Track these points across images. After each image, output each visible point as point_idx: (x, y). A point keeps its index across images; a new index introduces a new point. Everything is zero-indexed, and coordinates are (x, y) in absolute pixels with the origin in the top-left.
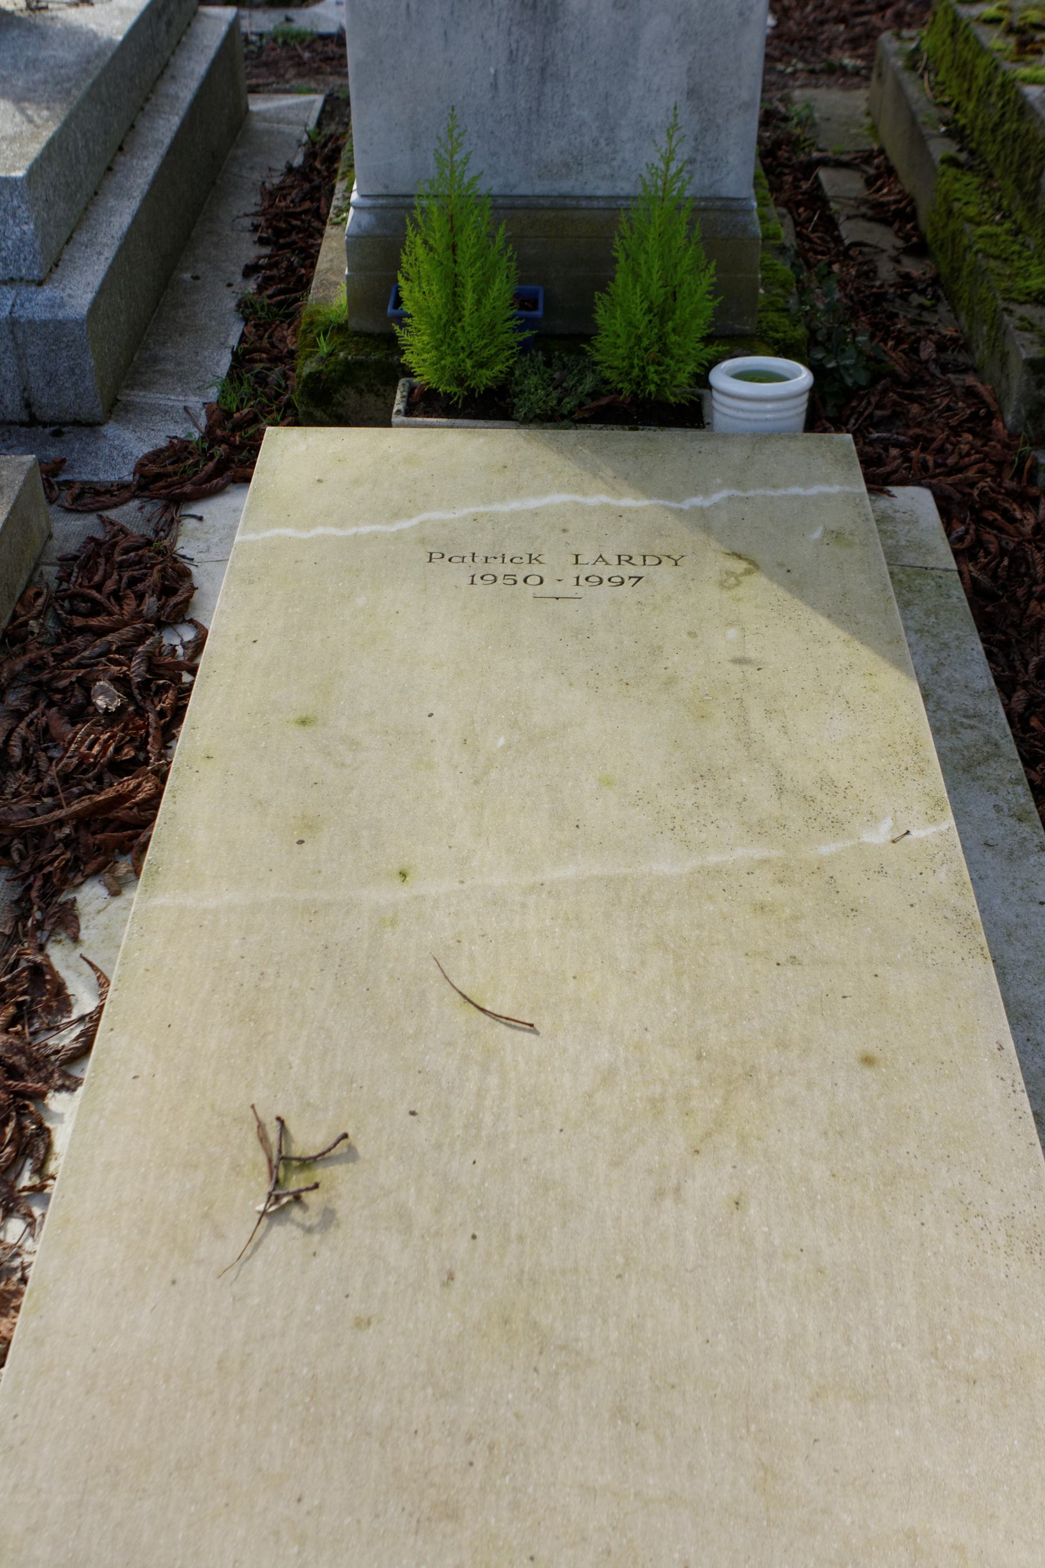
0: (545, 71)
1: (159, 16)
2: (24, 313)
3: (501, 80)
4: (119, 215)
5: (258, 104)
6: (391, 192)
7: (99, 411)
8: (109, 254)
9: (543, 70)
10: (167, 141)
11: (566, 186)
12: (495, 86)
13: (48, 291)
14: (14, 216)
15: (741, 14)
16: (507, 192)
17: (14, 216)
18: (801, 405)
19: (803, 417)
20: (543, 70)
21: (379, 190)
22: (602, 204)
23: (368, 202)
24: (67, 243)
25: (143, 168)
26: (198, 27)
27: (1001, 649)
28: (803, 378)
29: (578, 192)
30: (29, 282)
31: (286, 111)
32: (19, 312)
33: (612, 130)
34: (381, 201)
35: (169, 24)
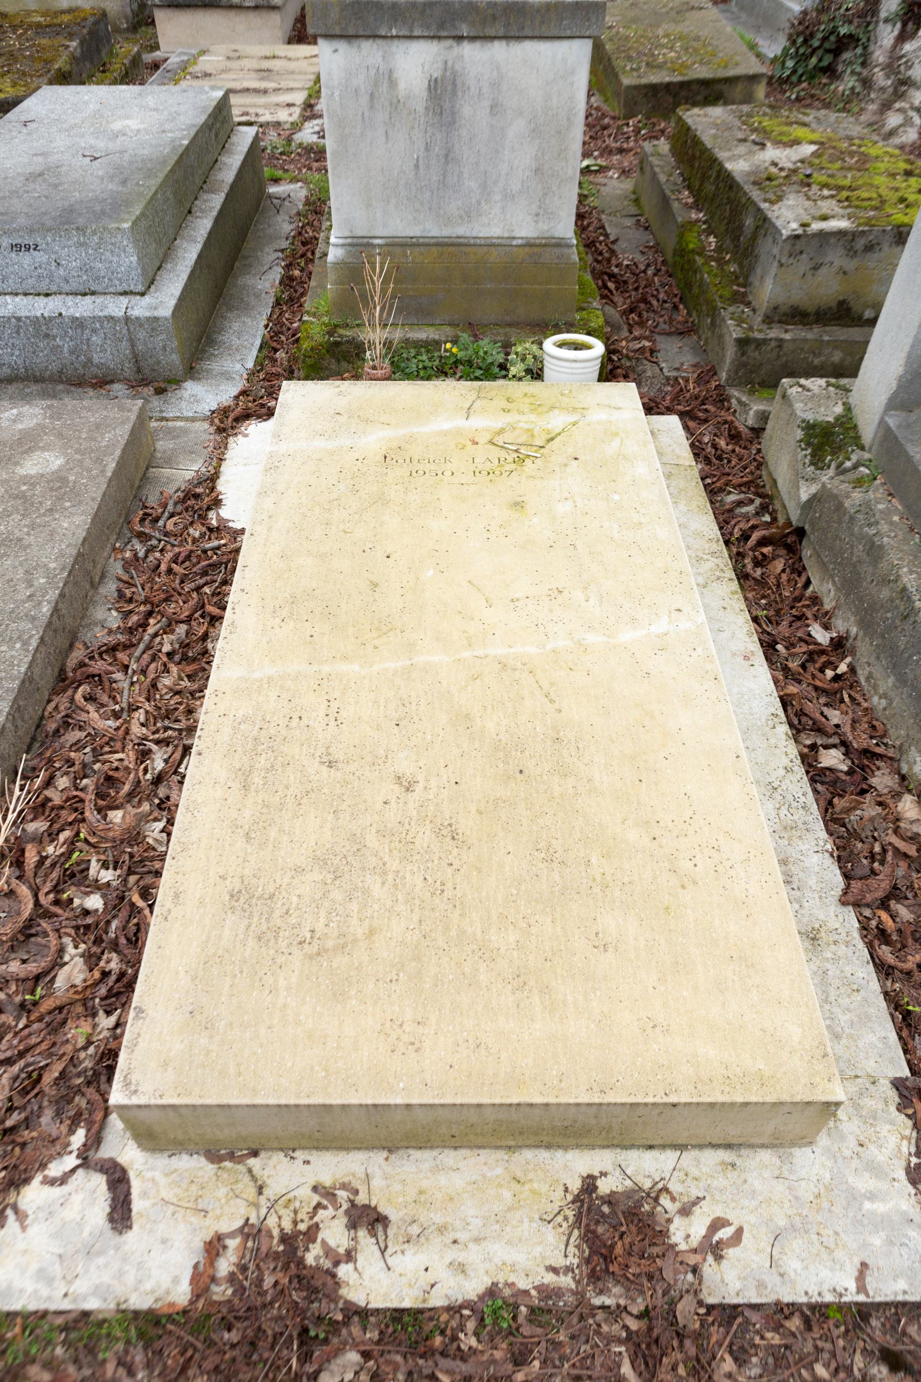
0: (448, 157)
1: (210, 130)
2: (136, 312)
3: (421, 162)
4: (189, 254)
5: (273, 189)
6: (354, 234)
7: (174, 360)
8: (184, 277)
9: (447, 156)
10: (219, 207)
11: (461, 231)
12: (417, 166)
13: (147, 299)
14: (124, 251)
15: (568, 119)
16: (426, 235)
17: (124, 251)
18: (596, 366)
19: (597, 373)
20: (447, 156)
21: (347, 234)
22: (483, 242)
23: (341, 241)
24: (159, 269)
25: (203, 226)
26: (234, 139)
27: (327, 1149)
28: (598, 348)
29: (468, 234)
30: (138, 294)
31: (293, 191)
32: (130, 312)
33: (489, 194)
34: (349, 240)
35: (217, 135)
